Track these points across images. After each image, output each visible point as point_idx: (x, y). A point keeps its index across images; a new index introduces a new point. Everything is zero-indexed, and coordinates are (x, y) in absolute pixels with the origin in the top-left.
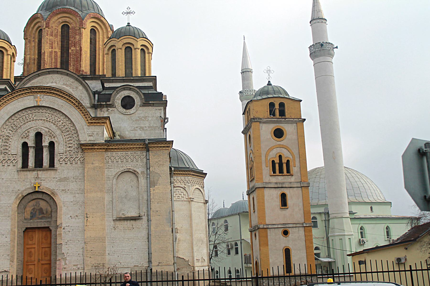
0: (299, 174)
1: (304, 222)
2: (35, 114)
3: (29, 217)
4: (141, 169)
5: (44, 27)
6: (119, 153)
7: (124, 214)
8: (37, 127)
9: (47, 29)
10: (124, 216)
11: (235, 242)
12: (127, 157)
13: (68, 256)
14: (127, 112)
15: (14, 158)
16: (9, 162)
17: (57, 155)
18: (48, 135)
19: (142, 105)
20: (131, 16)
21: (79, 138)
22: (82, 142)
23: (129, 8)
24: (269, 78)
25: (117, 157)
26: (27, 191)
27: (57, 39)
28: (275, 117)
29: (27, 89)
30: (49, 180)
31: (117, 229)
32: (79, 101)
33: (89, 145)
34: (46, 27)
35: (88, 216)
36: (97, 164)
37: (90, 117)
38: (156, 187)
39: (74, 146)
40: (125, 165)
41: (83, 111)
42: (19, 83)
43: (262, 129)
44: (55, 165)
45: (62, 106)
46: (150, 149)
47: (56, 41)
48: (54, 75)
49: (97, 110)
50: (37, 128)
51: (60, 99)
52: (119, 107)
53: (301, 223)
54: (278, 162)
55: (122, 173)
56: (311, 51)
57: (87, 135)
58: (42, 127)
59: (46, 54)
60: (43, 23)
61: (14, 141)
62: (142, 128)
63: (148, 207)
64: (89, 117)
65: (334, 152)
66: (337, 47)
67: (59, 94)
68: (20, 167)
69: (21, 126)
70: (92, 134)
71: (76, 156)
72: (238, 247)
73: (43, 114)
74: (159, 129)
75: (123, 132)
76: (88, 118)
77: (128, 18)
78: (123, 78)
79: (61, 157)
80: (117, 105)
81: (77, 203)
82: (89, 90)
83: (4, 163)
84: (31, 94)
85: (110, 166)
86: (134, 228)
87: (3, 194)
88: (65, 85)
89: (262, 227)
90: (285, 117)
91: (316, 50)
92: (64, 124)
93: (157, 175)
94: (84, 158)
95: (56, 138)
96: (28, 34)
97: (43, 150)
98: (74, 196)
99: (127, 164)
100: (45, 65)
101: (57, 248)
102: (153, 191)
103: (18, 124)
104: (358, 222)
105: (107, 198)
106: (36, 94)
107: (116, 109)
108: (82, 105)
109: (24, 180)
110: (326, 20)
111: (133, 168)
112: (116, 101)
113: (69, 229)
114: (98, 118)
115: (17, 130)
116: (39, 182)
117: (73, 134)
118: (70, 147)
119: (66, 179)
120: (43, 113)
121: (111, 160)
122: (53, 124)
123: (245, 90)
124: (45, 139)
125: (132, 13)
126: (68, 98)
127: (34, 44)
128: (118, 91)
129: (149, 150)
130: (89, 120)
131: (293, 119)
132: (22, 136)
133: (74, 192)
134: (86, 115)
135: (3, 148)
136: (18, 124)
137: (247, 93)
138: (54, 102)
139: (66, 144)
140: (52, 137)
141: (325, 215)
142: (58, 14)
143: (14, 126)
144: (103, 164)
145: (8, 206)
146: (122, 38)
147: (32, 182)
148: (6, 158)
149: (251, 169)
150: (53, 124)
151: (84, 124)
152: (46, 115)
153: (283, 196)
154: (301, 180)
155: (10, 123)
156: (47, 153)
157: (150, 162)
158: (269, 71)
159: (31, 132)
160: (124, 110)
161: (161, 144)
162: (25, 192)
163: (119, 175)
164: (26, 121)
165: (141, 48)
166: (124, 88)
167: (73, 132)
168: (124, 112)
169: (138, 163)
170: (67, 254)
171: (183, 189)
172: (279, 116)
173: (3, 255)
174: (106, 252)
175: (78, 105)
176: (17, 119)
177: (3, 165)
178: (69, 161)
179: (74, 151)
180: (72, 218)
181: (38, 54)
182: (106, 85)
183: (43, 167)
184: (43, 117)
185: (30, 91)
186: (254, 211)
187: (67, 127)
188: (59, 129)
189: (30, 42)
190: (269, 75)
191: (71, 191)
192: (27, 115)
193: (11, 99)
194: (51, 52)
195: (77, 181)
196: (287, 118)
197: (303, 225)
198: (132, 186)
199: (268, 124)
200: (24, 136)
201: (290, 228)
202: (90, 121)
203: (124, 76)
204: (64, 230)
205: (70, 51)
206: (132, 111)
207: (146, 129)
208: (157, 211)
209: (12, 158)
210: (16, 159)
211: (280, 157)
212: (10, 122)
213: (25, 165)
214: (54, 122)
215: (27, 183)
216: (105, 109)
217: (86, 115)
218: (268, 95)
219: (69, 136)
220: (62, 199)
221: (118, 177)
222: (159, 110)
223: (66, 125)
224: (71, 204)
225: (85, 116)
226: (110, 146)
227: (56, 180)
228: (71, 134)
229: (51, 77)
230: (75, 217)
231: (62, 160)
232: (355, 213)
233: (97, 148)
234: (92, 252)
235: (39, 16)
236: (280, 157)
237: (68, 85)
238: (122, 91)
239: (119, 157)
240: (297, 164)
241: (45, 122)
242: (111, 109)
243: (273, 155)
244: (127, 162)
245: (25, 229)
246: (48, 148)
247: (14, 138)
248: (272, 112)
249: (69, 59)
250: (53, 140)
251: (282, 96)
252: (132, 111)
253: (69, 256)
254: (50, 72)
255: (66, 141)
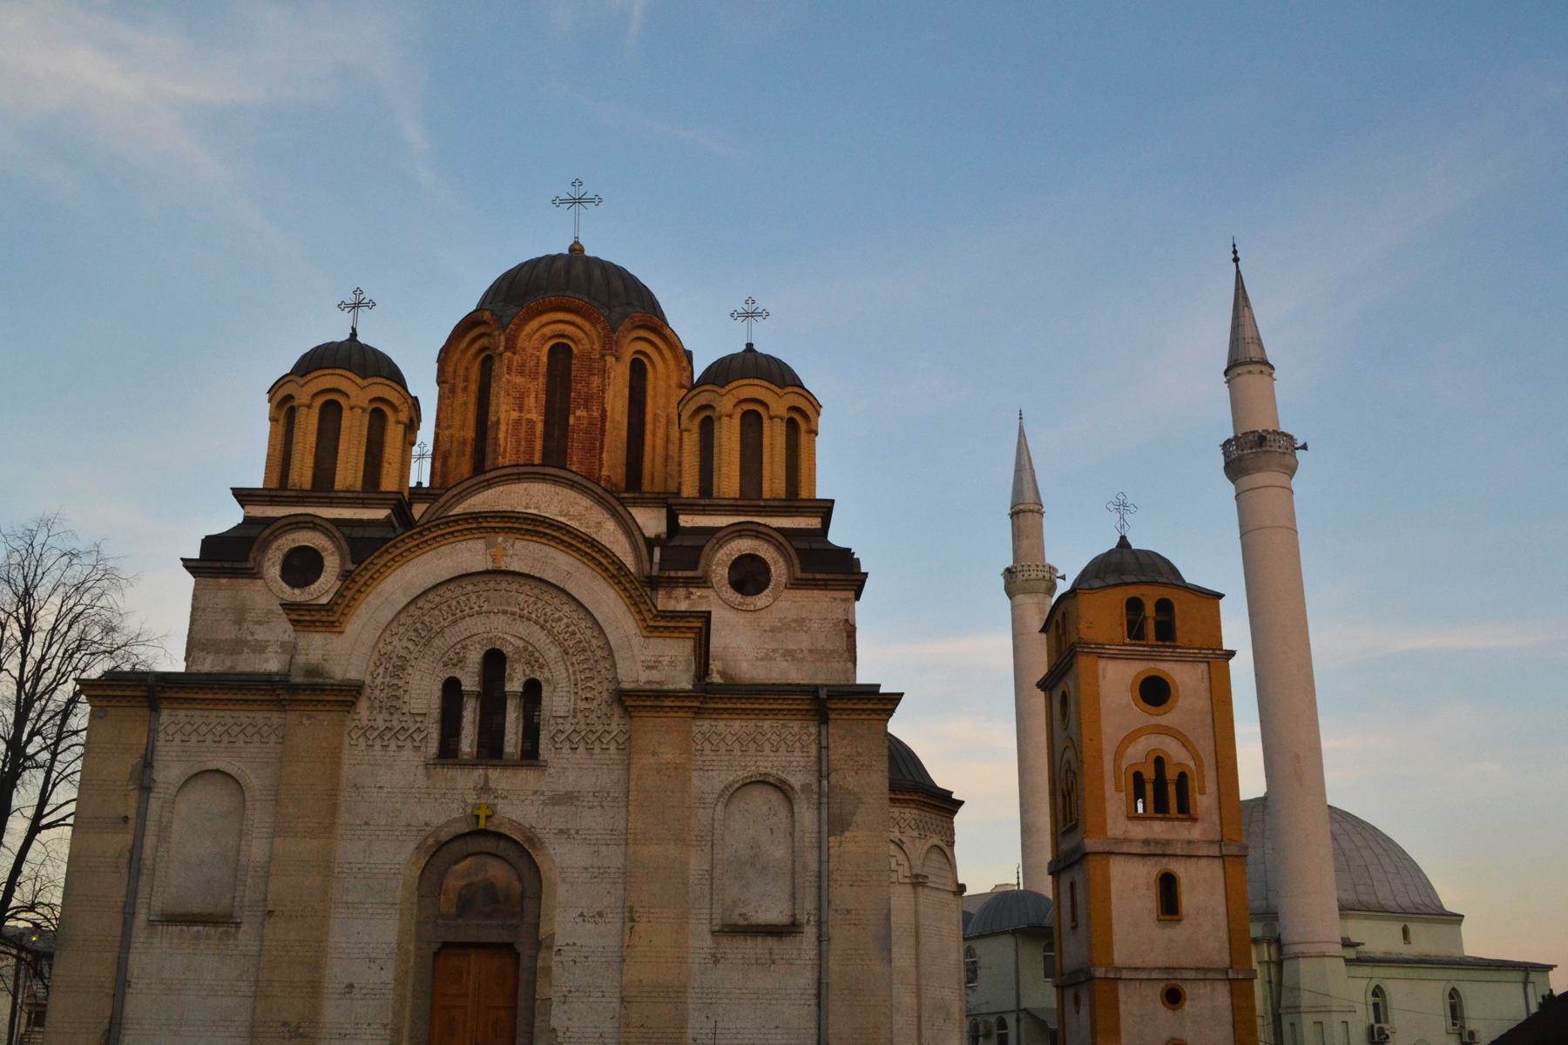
0: (1216, 818)
1: (1231, 967)
2: (485, 594)
3: (453, 910)
4: (802, 778)
5: (501, 349)
6: (738, 725)
7: (745, 914)
8: (490, 635)
9: (508, 354)
10: (745, 923)
11: (997, 1016)
12: (759, 736)
13: (567, 1040)
14: (748, 604)
15: (418, 725)
16: (402, 738)
17: (549, 721)
18: (523, 660)
19: (792, 584)
20: (758, 325)
21: (616, 673)
22: (626, 686)
23: (750, 302)
24: (1122, 527)
25: (729, 737)
26: (452, 830)
27: (535, 383)
28: (1145, 643)
29: (456, 521)
30: (521, 798)
31: (722, 960)
32: (621, 561)
33: (647, 696)
34: (506, 349)
35: (636, 916)
36: (668, 755)
37: (653, 609)
38: (846, 833)
39: (601, 697)
40: (753, 763)
41: (632, 592)
42: (429, 507)
43: (1104, 677)
44: (541, 752)
45: (569, 573)
46: (831, 717)
47: (532, 390)
48: (532, 484)
49: (657, 594)
50: (491, 638)
51: (564, 552)
52: (724, 589)
53: (1220, 969)
54: (1153, 777)
55: (745, 785)
56: (1228, 454)
57: (639, 664)
58: (505, 636)
59: (503, 427)
60: (499, 339)
61: (421, 673)
62: (789, 654)
63: (820, 897)
64: (650, 610)
65: (1297, 756)
66: (1304, 447)
67: (562, 537)
68: (434, 754)
69: (442, 630)
70: (655, 662)
71: (606, 728)
72: (1006, 1034)
73: (512, 596)
74: (840, 658)
75: (732, 663)
76: (645, 614)
77: (749, 332)
78: (735, 503)
79: (560, 727)
80: (717, 583)
81: (603, 874)
82: (636, 533)
83: (386, 738)
84: (476, 536)
85: (707, 763)
86: (777, 961)
87: (377, 833)
88: (565, 516)
89: (1103, 976)
90: (1172, 644)
91: (1245, 452)
92: (570, 629)
93: (852, 797)
94: (629, 734)
95: (546, 670)
96: (450, 369)
97: (506, 704)
98: (595, 852)
99: (759, 758)
100: (498, 458)
101: (537, 1012)
102: (836, 849)
103: (433, 621)
104: (1365, 971)
105: (697, 862)
106: (492, 534)
107: (712, 594)
108: (628, 573)
109: (444, 795)
110: (1272, 367)
111: (777, 774)
112: (715, 570)
113: (574, 954)
114: (675, 614)
115: (429, 642)
116: (490, 801)
117: (596, 661)
118: (587, 699)
119: (568, 798)
120: (510, 594)
121: (709, 745)
122: (538, 626)
123: (1023, 566)
124: (514, 670)
125: (760, 314)
126: (589, 551)
127: (467, 399)
128: (721, 538)
129: (828, 719)
130: (648, 619)
131: (1197, 651)
132: (445, 659)
133: (595, 837)
134: (640, 602)
135: (388, 693)
136: (433, 621)
137: (1026, 574)
138: (544, 560)
139: (576, 691)
140: (536, 668)
141: (1269, 947)
142: (540, 313)
143: (424, 630)
144: (685, 756)
145: (392, 871)
146: (734, 386)
147: (469, 801)
148: (395, 723)
149: (1064, 797)
150: (538, 626)
151: (634, 632)
152: (520, 599)
153: (1168, 887)
154: (1222, 836)
155: (410, 618)
156: (516, 714)
157: (832, 757)
158: (1122, 507)
159: (471, 648)
160: (737, 598)
161: (866, 701)
162: (446, 829)
163: (734, 792)
164: (459, 614)
165: (786, 415)
166: (739, 531)
167: (599, 653)
168: (737, 603)
169: (792, 759)
170: (564, 1033)
171: (897, 847)
172: (1154, 638)
173: (369, 1025)
174: (685, 1033)
175: (613, 571)
176: (433, 609)
177: (384, 744)
178: (582, 741)
179: (599, 711)
180: (584, 921)
181: (477, 426)
182: (686, 521)
183: (504, 757)
184: (509, 604)
185: (474, 525)
186: (1074, 924)
187: (582, 637)
188: (556, 643)
189: (453, 391)
190: (1122, 517)
191: (584, 836)
192: (463, 598)
193: (417, 545)
194: (518, 422)
195: (604, 804)
196: (1179, 647)
197: (1227, 974)
198: (771, 830)
199: (1125, 661)
200: (451, 659)
201: (1188, 982)
202: (651, 623)
203: (738, 496)
204: (560, 955)
205: (572, 420)
206: (762, 600)
207: (800, 656)
208: (849, 912)
209: (411, 724)
210: (422, 728)
211: (1159, 762)
212: (411, 615)
213: (448, 752)
214: (541, 620)
215: (453, 802)
216: (680, 592)
217: (640, 602)
218: (1123, 577)
219: (585, 666)
220: (557, 860)
221: (729, 798)
222: (842, 600)
223: (577, 630)
224: (584, 875)
225: (638, 607)
226: (708, 700)
227: (542, 798)
228: (592, 661)
229: (525, 490)
230: (594, 916)
231: (564, 736)
232: (1358, 944)
233: (671, 707)
234: (642, 1030)
235: (485, 318)
236: (1159, 762)
237: (574, 516)
238: (733, 539)
239: (735, 738)
240: (1211, 787)
241: (514, 620)
242: (699, 594)
243: (1138, 751)
244: (760, 753)
245: (438, 945)
246: (520, 701)
247: (421, 664)
248: (1135, 631)
249: (567, 445)
250: (537, 676)
251: (1164, 580)
252: (763, 601)
253: (572, 1040)
254: (521, 473)
255: (576, 679)
